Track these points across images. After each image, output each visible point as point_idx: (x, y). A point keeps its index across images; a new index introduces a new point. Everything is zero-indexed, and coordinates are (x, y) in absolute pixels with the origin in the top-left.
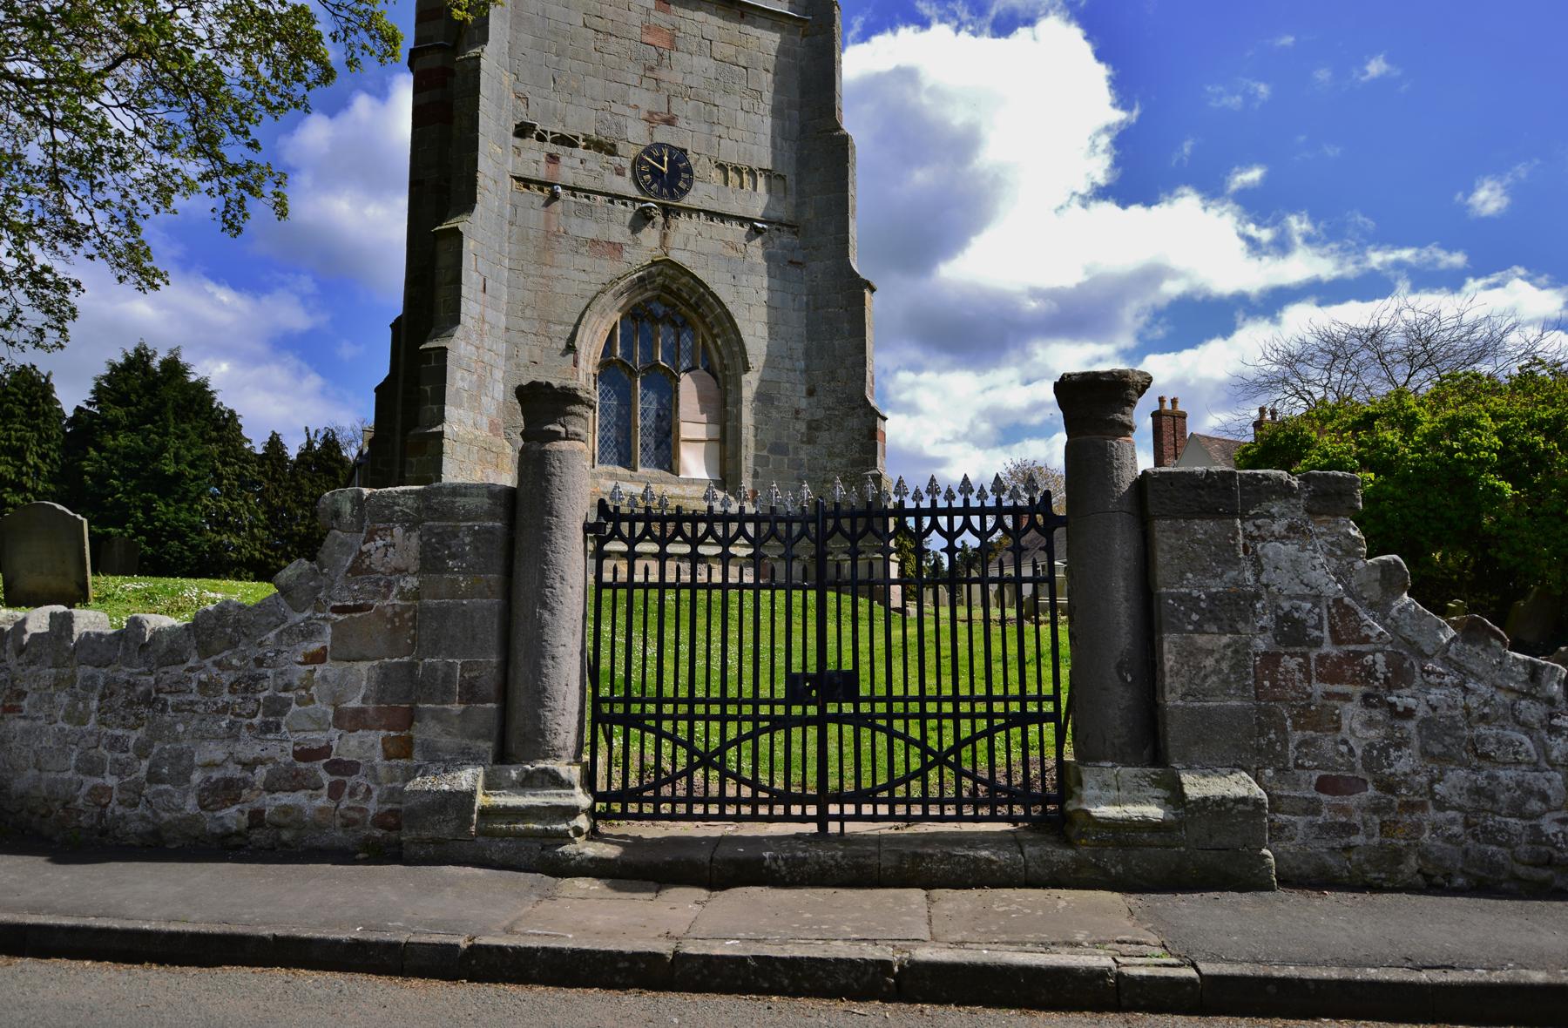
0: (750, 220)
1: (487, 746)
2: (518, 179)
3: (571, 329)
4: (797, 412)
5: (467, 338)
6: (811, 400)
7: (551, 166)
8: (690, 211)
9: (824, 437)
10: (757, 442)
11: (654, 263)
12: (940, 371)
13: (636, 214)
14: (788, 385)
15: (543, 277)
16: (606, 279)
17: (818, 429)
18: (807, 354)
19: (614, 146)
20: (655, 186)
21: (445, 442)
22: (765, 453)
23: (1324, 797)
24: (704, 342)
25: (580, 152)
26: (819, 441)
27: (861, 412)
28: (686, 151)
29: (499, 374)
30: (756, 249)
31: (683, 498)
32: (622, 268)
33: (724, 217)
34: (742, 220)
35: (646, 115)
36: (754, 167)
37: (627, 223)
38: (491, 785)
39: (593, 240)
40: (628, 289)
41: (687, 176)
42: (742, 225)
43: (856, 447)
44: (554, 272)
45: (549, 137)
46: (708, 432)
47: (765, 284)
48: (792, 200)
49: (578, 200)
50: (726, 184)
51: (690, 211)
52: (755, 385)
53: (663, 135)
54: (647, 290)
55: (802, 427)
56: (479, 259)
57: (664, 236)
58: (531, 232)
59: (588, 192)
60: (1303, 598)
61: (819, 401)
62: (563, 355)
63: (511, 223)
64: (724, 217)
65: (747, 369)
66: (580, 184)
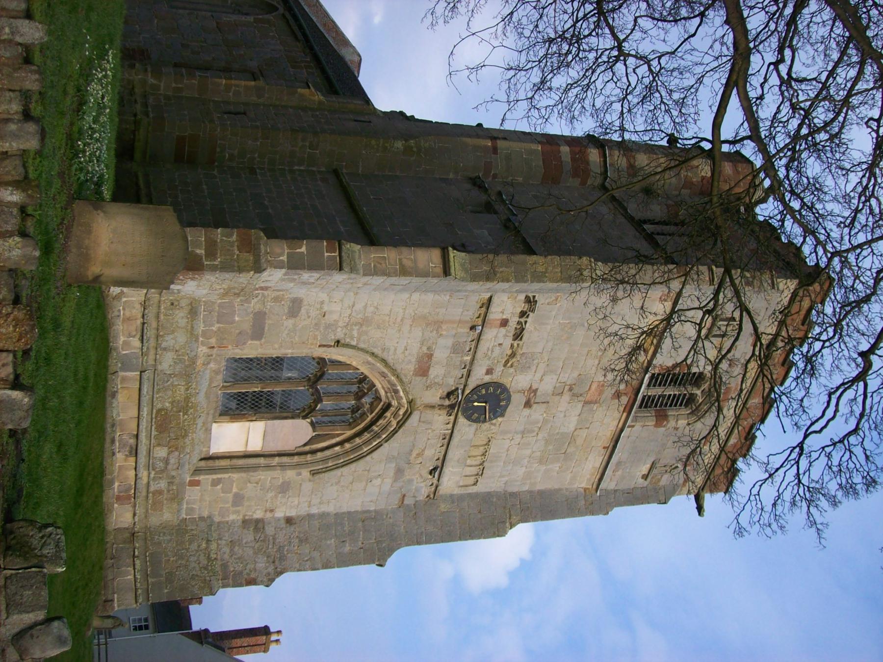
3: (354, 343)
4: (272, 511)
6: (283, 522)
7: (499, 322)
9: (249, 536)
12: (295, 265)
14: (296, 502)
15: (402, 320)
17: (256, 529)
18: (323, 515)
24: (338, 435)
25: (509, 341)
26: (245, 531)
27: (271, 569)
35: (534, 388)
39: (432, 355)
43: (240, 567)
44: (405, 329)
45: (523, 320)
48: (457, 491)
53: (517, 400)
55: (259, 515)
61: (281, 529)
66: (482, 342)
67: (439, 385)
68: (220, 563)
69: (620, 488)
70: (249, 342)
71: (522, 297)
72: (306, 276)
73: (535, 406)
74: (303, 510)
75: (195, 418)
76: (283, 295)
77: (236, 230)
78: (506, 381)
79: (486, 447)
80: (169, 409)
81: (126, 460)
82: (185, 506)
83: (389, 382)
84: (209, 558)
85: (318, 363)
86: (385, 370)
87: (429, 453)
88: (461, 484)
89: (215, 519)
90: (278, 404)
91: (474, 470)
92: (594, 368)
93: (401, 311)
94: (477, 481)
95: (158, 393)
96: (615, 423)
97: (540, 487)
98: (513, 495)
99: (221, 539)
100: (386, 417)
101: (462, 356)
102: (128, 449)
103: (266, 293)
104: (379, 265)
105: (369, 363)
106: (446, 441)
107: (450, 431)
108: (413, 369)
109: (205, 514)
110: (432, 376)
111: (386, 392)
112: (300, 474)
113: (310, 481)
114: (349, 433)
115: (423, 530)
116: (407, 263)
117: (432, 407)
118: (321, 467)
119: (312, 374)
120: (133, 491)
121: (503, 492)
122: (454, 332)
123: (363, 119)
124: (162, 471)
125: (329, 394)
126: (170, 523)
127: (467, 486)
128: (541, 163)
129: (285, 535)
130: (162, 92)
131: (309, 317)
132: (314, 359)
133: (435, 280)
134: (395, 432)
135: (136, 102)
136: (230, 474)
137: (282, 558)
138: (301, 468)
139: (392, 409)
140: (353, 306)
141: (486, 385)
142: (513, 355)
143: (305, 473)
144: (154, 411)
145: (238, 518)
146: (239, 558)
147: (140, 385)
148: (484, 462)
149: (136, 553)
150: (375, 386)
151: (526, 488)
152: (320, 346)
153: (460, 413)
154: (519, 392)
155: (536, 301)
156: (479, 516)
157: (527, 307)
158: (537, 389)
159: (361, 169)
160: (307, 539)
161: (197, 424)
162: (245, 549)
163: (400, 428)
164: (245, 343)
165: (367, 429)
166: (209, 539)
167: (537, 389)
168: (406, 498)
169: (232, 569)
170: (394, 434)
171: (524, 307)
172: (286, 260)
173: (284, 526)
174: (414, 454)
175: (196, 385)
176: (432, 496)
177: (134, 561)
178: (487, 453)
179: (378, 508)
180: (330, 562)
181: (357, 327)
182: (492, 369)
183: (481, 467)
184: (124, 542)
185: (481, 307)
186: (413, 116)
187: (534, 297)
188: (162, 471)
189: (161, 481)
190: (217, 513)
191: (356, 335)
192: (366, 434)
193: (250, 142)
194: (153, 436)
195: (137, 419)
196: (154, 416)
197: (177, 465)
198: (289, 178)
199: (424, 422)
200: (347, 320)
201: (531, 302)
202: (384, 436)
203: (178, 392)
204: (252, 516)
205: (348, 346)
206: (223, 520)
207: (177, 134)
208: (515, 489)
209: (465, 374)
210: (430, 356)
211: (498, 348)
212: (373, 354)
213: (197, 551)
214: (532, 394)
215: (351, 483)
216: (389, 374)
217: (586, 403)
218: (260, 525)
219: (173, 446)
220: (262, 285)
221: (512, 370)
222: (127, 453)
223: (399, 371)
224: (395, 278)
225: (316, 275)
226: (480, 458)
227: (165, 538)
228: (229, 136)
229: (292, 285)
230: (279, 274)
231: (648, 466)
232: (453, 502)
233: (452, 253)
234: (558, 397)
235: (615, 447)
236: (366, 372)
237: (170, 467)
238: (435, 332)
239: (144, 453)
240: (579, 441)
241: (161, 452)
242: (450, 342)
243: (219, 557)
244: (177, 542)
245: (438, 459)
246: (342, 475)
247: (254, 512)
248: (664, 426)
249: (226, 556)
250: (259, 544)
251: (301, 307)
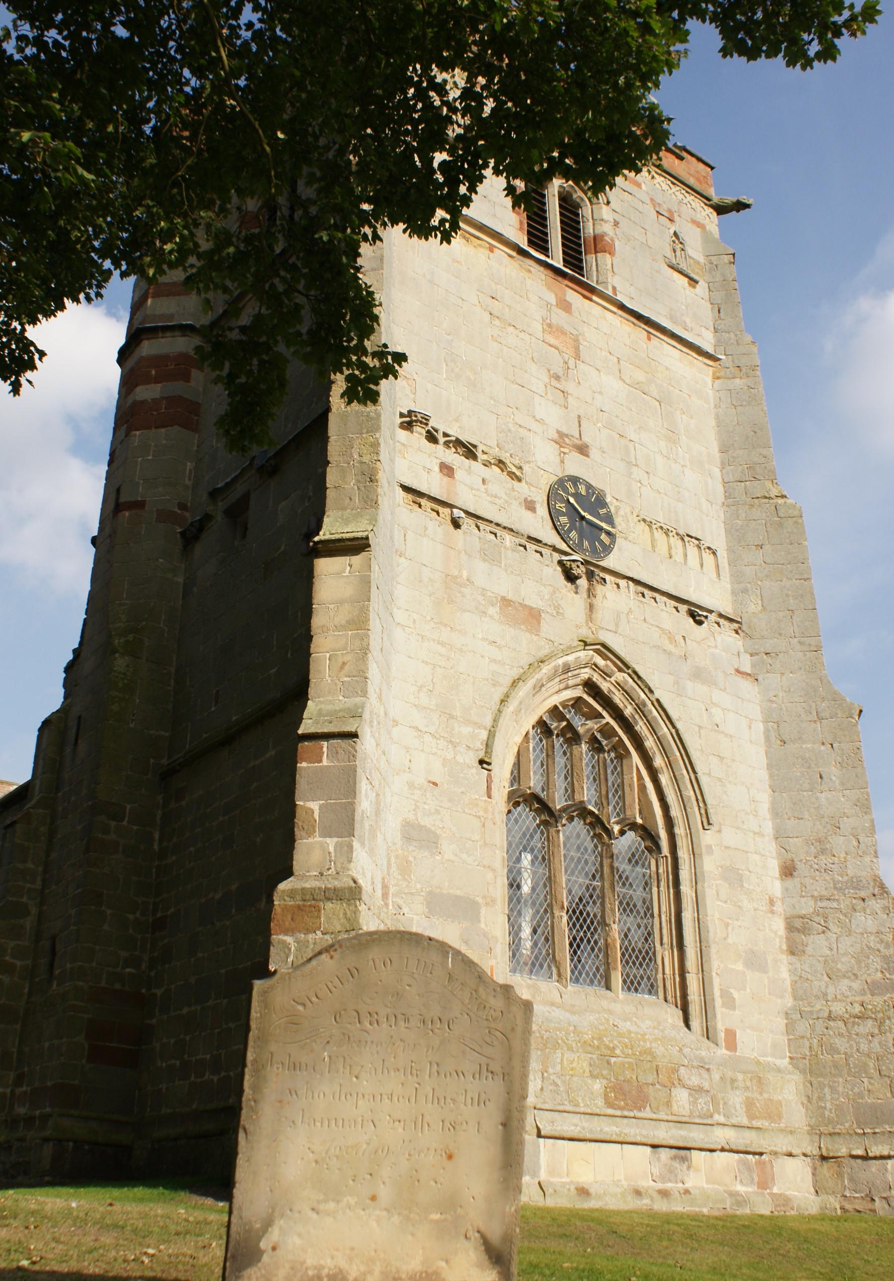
3: (484, 735)
4: (772, 902)
6: (790, 883)
9: (817, 944)
14: (757, 857)
17: (805, 930)
18: (775, 813)
24: (640, 777)
26: (809, 950)
39: (503, 599)
45: (442, 440)
48: (726, 582)
53: (575, 466)
55: (779, 925)
67: (554, 592)
68: (868, 998)
69: (712, 324)
70: (483, 926)
71: (403, 434)
72: (365, 804)
73: (586, 439)
74: (771, 847)
75: (620, 1035)
76: (397, 857)
77: (274, 937)
78: (546, 481)
79: (654, 527)
80: (605, 1082)
81: (697, 1170)
82: (769, 1059)
83: (550, 679)
84: (861, 1017)
85: (517, 804)
86: (531, 683)
87: (667, 624)
88: (714, 575)
89: (790, 1005)
90: (587, 882)
91: (692, 551)
92: (522, 335)
94: (709, 548)
95: (577, 1105)
96: (609, 315)
97: (715, 448)
98: (728, 495)
99: (825, 995)
100: (610, 691)
101: (505, 547)
102: (676, 1164)
103: (392, 890)
104: (347, 667)
105: (518, 711)
106: (646, 592)
107: (630, 583)
108: (528, 635)
109: (781, 1022)
110: (540, 602)
111: (567, 688)
112: (709, 847)
113: (720, 831)
114: (636, 758)
115: (796, 640)
116: (343, 615)
117: (591, 607)
118: (696, 809)
119: (534, 819)
120: (750, 1157)
121: (727, 509)
123: (74, 731)
124: (713, 1099)
125: (571, 790)
126: (801, 1087)
127: (717, 566)
128: (163, 430)
129: (814, 878)
130: (8, 1091)
131: (437, 812)
132: (509, 812)
133: (375, 567)
134: (636, 676)
135: (22, 1140)
136: (714, 974)
137: (855, 884)
138: (700, 845)
139: (596, 678)
140: (417, 729)
142: (501, 463)
143: (707, 838)
144: (610, 1111)
145: (785, 962)
146: (859, 962)
147: (563, 1139)
148: (677, 534)
149: (860, 1152)
150: (556, 707)
151: (717, 472)
152: (489, 797)
153: (600, 563)
154: (562, 462)
155: (410, 412)
156: (767, 547)
157: (419, 429)
158: (558, 432)
159: (162, 733)
161: (630, 1032)
162: (841, 951)
163: (628, 667)
164: (485, 935)
165: (628, 726)
166: (826, 1015)
167: (558, 432)
168: (742, 669)
169: (879, 975)
170: (639, 677)
171: (421, 434)
172: (335, 840)
173: (797, 880)
174: (670, 647)
175: (560, 1030)
176: (736, 626)
177: (875, 1158)
178: (665, 527)
179: (759, 716)
180: (858, 800)
181: (456, 725)
182: (526, 500)
183: (687, 539)
184: (840, 1175)
185: (420, 506)
186: (75, 651)
187: (402, 415)
188: (713, 1099)
189: (730, 1103)
190: (779, 1001)
191: (470, 729)
192: (637, 728)
193: (106, 927)
194: (654, 1116)
195: (625, 1146)
196: (618, 1113)
197: (702, 1071)
198: (174, 858)
199: (617, 625)
200: (442, 743)
201: (410, 421)
202: (643, 696)
203: (574, 1065)
204: (781, 937)
205: (488, 746)
206: (790, 989)
207: (84, 1061)
208: (720, 489)
209: (535, 547)
210: (506, 602)
211: (490, 486)
212: (502, 701)
213: (850, 1037)
214: (567, 440)
215: (722, 759)
216: (538, 676)
217: (578, 357)
218: (798, 923)
219: (669, 1077)
220: (379, 893)
221: (526, 468)
222: (685, 1166)
223: (531, 660)
224: (372, 637)
225: (363, 786)
226: (672, 540)
227: (828, 1097)
228: (94, 964)
229: (380, 838)
230: (360, 854)
231: (676, 275)
232: (745, 591)
233: (324, 535)
234: (570, 399)
235: (647, 321)
236: (534, 719)
237: (706, 1086)
238: (463, 590)
239: (683, 1133)
240: (640, 376)
241: (681, 1098)
242: (481, 567)
243: (859, 999)
244: (835, 1076)
245: (676, 608)
246: (709, 774)
247: (775, 933)
248: (612, 240)
249: (856, 985)
250: (831, 926)
251: (419, 826)
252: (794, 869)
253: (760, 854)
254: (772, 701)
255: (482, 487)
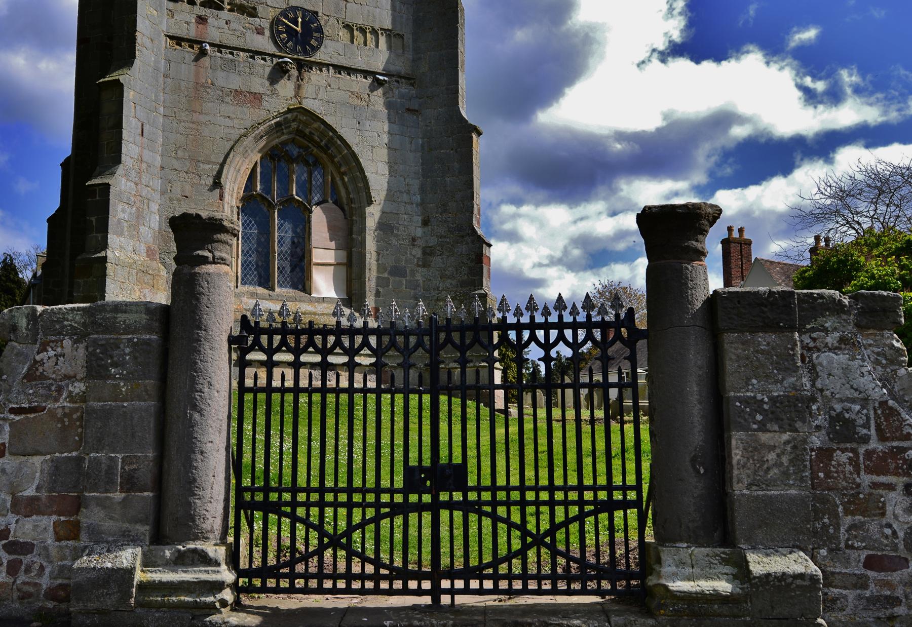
0: (373, 74)
1: (144, 529)
2: (172, 38)
5: (127, 176)
6: (426, 229)
7: (200, 26)
8: (321, 65)
10: (379, 265)
11: (289, 111)
13: (274, 68)
14: (406, 216)
16: (248, 125)
17: (432, 254)
19: (254, 9)
20: (290, 43)
21: (108, 265)
22: (386, 275)
23: (871, 574)
26: (433, 264)
27: (469, 239)
28: (317, 13)
29: (155, 207)
30: (378, 99)
31: (315, 314)
32: (263, 115)
33: (350, 71)
34: (366, 73)
36: (376, 27)
37: (266, 76)
38: (148, 563)
39: (236, 91)
40: (267, 133)
41: (318, 35)
42: (366, 78)
44: (203, 119)
46: (336, 258)
47: (386, 128)
48: (409, 55)
49: (224, 55)
50: (352, 42)
51: (321, 65)
52: (377, 216)
54: (283, 134)
55: (418, 252)
56: (138, 107)
57: (298, 87)
58: (183, 84)
59: (233, 49)
60: (853, 401)
62: (211, 190)
63: (166, 76)
64: (350, 71)
65: (370, 202)
66: (226, 42)
88: (401, 51)
93: (183, 124)
122: (209, 70)
141: (273, 38)
146: (457, 270)
160: (443, 205)
166: (435, 298)
180: (467, 181)
204: (418, 258)
218: (428, 251)
238: (208, 90)
249: (454, 282)
252: (429, 221)
253: (409, 214)
254: (427, 126)
255: (226, 27)
